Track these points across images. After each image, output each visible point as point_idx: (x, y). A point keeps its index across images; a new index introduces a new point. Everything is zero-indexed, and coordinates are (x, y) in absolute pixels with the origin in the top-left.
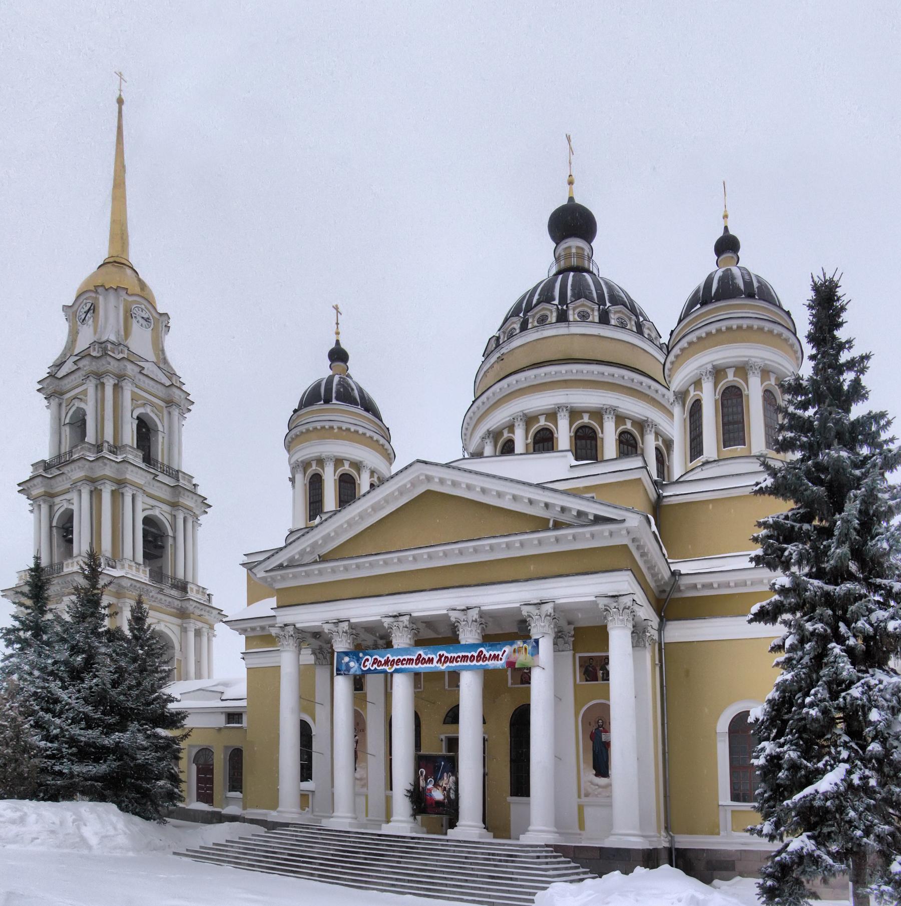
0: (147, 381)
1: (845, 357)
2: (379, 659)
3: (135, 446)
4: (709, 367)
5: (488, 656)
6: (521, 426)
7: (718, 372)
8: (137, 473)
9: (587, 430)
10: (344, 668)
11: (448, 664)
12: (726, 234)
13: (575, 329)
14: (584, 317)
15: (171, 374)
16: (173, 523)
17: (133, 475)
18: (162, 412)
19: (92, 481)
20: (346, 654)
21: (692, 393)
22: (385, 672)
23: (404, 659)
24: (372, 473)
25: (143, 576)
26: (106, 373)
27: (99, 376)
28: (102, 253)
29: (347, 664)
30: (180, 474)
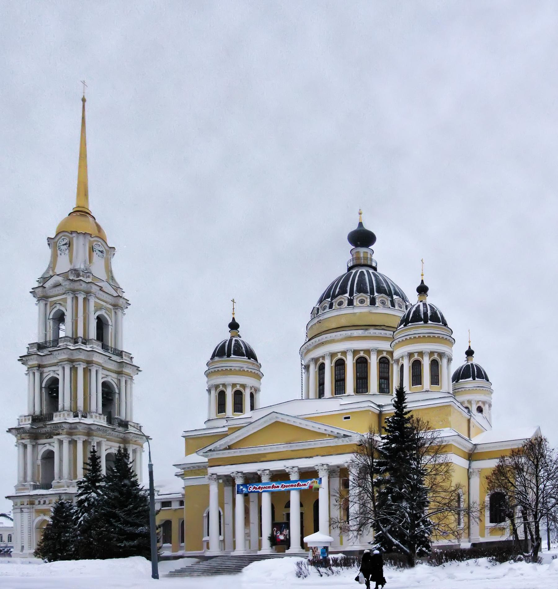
0: (106, 295)
1: (405, 410)
2: (256, 487)
3: (96, 339)
4: (406, 354)
5: (301, 484)
6: (328, 358)
7: (410, 355)
8: (99, 357)
9: (362, 359)
10: (240, 491)
11: (285, 488)
12: (422, 285)
13: (356, 310)
14: (362, 302)
15: (117, 288)
16: (118, 384)
17: (96, 358)
18: (111, 313)
19: (71, 361)
20: (242, 485)
21: (401, 361)
22: (258, 492)
23: (267, 487)
24: (251, 388)
25: (102, 421)
26: (79, 291)
27: (74, 292)
28: (72, 205)
29: (242, 489)
30: (124, 353)
